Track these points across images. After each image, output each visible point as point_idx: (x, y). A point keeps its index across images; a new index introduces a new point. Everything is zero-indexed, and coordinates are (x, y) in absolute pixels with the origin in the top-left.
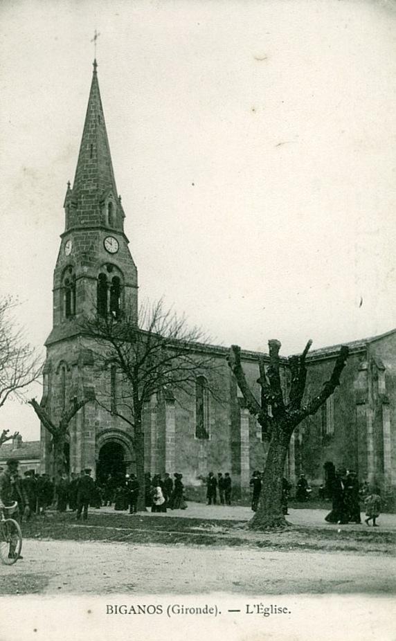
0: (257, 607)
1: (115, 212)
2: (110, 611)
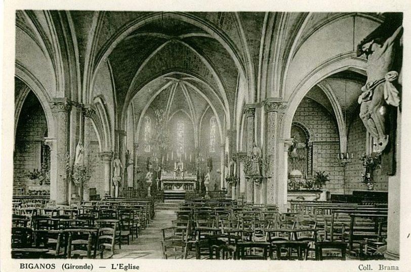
0: (119, 265)
1: (249, 60)
2: (382, 268)
